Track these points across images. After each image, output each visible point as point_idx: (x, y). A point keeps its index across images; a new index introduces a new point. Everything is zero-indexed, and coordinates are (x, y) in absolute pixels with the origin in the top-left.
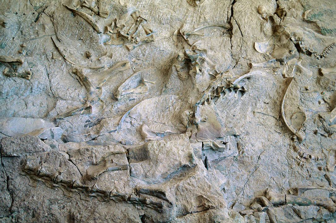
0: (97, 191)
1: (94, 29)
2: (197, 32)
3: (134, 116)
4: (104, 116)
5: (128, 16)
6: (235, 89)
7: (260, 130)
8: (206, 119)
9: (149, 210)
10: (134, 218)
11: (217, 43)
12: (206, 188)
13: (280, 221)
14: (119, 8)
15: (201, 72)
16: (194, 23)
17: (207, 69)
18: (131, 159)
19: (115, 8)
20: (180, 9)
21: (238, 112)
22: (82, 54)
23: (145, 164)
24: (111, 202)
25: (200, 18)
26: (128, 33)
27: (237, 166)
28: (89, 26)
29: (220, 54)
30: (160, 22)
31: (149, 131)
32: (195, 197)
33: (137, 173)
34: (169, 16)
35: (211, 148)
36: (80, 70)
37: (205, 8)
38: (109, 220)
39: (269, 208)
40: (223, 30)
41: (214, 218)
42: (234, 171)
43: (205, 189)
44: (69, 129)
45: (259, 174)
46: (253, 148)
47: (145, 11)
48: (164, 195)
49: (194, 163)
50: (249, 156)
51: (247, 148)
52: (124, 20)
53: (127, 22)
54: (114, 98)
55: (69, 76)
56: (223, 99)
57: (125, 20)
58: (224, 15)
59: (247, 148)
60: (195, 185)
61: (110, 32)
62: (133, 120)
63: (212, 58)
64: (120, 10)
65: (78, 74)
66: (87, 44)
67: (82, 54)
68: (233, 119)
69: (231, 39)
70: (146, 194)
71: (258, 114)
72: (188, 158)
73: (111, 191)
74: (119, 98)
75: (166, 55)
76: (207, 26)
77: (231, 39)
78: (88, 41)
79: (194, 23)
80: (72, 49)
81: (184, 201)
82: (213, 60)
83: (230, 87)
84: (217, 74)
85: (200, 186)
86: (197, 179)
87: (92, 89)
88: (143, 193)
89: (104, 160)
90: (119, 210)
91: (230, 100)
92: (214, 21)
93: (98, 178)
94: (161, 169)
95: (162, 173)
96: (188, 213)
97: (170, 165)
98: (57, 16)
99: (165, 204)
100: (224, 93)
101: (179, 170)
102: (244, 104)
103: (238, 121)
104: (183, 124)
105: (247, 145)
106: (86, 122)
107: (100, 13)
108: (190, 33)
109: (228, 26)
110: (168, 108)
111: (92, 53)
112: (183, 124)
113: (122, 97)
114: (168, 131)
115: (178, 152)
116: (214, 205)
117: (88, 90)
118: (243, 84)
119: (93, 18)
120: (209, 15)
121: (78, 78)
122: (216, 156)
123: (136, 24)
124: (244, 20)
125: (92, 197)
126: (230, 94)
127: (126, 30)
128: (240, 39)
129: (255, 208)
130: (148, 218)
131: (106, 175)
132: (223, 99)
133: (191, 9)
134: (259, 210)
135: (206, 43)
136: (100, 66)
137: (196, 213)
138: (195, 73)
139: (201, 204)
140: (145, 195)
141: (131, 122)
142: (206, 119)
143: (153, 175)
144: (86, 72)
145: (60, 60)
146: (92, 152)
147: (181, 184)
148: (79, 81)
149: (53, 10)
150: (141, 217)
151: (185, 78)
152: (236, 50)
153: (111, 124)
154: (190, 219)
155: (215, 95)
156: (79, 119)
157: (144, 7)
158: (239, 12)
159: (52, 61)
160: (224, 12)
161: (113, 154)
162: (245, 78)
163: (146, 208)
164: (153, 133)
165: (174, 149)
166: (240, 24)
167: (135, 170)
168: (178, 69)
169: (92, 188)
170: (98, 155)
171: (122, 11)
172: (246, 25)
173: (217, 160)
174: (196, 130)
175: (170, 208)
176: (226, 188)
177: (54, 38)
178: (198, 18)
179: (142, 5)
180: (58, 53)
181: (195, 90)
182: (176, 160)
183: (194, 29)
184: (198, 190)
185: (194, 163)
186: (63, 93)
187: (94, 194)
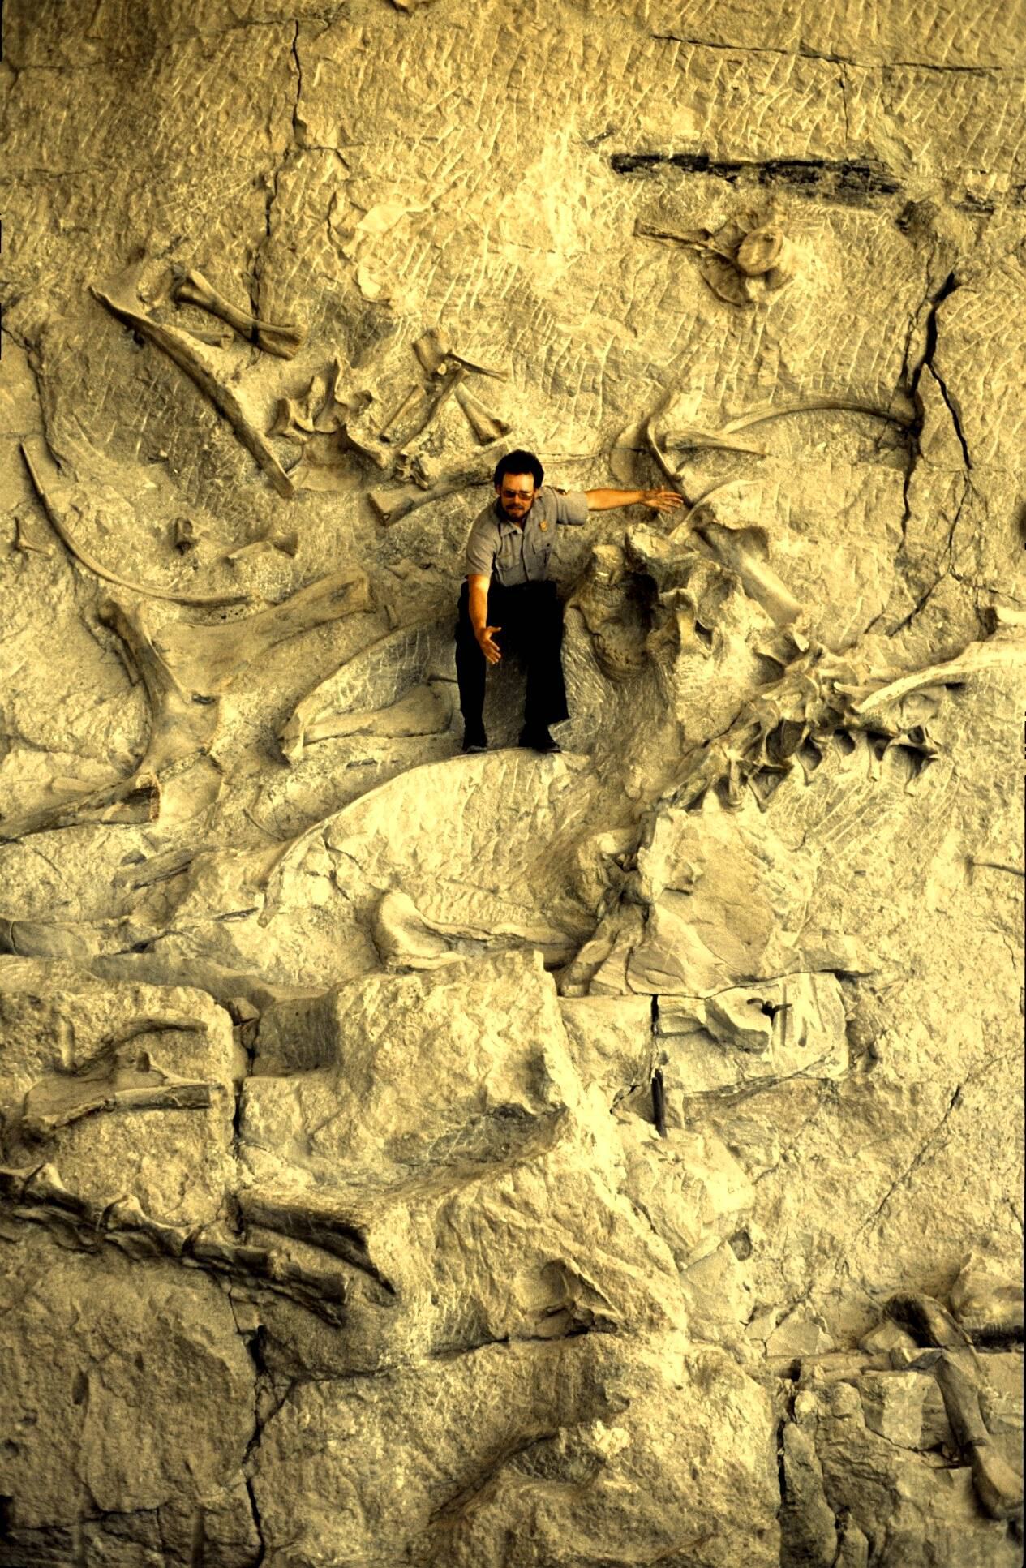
0: (53, 1199)
1: (221, 412)
2: (736, 437)
3: (346, 846)
4: (212, 839)
5: (394, 354)
6: (877, 737)
7: (987, 955)
8: (690, 882)
9: (284, 1308)
10: (204, 1340)
11: (833, 497)
12: (594, 1226)
13: (1005, 1420)
14: (352, 313)
15: (710, 641)
16: (729, 388)
17: (744, 627)
18: (264, 1057)
19: (334, 309)
20: (663, 316)
21: (886, 855)
22: (156, 532)
23: (318, 1090)
24: (113, 1256)
25: (760, 362)
26: (387, 435)
27: (835, 1129)
28: (194, 397)
29: (840, 550)
30: (556, 383)
31: (411, 926)
32: (531, 1263)
33: (274, 1127)
34: (601, 355)
35: (702, 1031)
36: (127, 612)
37: (790, 317)
38: (89, 1337)
39: (952, 1357)
40: (877, 429)
41: (604, 1377)
42: (814, 1150)
43: (589, 1231)
44: (42, 892)
45: (940, 1179)
46: (930, 1045)
47: (483, 325)
48: (361, 1244)
49: (552, 1097)
50: (901, 1083)
51: (898, 1043)
52: (372, 368)
53: (386, 379)
54: (272, 747)
55: (80, 637)
56: (807, 783)
57: (379, 371)
58: (888, 355)
59: (898, 1043)
60: (540, 1203)
61: (297, 426)
62: (345, 861)
63: (794, 569)
64: (359, 318)
65: (121, 628)
66: (185, 483)
67: (156, 532)
68: (855, 887)
69: (908, 474)
70: (277, 1230)
71: (989, 872)
72: (522, 1072)
73: (110, 1200)
74: (295, 752)
75: (565, 550)
76: (795, 403)
77: (908, 474)
78: (190, 470)
79: (729, 388)
80: (111, 506)
81: (476, 1281)
82: (798, 583)
83: (841, 725)
84: (793, 652)
85: (563, 1211)
86: (551, 1180)
87: (174, 705)
88: (263, 1226)
89: (108, 1050)
90: (137, 1295)
91: (842, 794)
92: (828, 380)
93: (64, 1139)
94: (386, 1114)
95: (388, 1136)
96: (487, 1338)
97: (432, 1099)
98: (56, 345)
99: (357, 1287)
100: (813, 752)
101: (481, 1126)
102: (921, 817)
103: (879, 902)
104: (579, 899)
105: (904, 1027)
106: (125, 861)
107: (264, 337)
108: (699, 441)
109: (900, 407)
110: (527, 814)
111: (203, 525)
112: (579, 899)
113: (313, 748)
114: (510, 928)
115: (477, 1042)
116: (615, 1315)
117: (154, 706)
118: (914, 715)
119: (219, 360)
120: (807, 354)
121: (120, 646)
122: (725, 1071)
123: (430, 391)
124: (987, 382)
125: (31, 1226)
126: (847, 761)
127: (377, 419)
128: (955, 483)
129: (878, 1351)
130: (280, 1346)
131: (105, 1126)
132: (807, 783)
133: (719, 319)
134: (895, 1364)
135: (774, 492)
136: (234, 590)
137: (529, 1345)
138: (674, 645)
139: (557, 1303)
140: (272, 1237)
141: (333, 877)
142: (690, 882)
143: (345, 1144)
144: (159, 622)
145: (49, 559)
146: (55, 1013)
147: (466, 1198)
148: (122, 663)
149: (41, 317)
150: (249, 1338)
151: (628, 671)
152: (923, 535)
153: (230, 879)
154: (489, 1368)
155: (764, 761)
156: (93, 847)
157: (479, 306)
158: (967, 341)
159: (11, 562)
160: (887, 339)
161: (157, 1028)
162: (933, 684)
163: (270, 1297)
164: (433, 933)
165: (463, 1027)
166: (964, 405)
167: (264, 1111)
168: (595, 622)
169: (30, 1180)
170: (83, 1031)
171: (364, 328)
172: (994, 407)
173: (728, 1088)
174: (635, 935)
175: (383, 1310)
176: (757, 1233)
177: (34, 449)
178: (750, 367)
179: (469, 295)
180: (42, 522)
181: (670, 729)
182: (462, 1078)
183: (725, 417)
184: (549, 1233)
185: (552, 1097)
186: (39, 717)
187: (33, 1212)
